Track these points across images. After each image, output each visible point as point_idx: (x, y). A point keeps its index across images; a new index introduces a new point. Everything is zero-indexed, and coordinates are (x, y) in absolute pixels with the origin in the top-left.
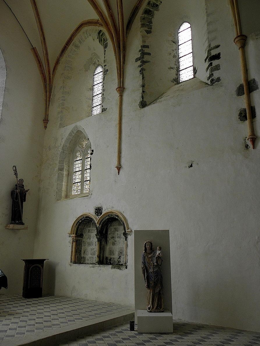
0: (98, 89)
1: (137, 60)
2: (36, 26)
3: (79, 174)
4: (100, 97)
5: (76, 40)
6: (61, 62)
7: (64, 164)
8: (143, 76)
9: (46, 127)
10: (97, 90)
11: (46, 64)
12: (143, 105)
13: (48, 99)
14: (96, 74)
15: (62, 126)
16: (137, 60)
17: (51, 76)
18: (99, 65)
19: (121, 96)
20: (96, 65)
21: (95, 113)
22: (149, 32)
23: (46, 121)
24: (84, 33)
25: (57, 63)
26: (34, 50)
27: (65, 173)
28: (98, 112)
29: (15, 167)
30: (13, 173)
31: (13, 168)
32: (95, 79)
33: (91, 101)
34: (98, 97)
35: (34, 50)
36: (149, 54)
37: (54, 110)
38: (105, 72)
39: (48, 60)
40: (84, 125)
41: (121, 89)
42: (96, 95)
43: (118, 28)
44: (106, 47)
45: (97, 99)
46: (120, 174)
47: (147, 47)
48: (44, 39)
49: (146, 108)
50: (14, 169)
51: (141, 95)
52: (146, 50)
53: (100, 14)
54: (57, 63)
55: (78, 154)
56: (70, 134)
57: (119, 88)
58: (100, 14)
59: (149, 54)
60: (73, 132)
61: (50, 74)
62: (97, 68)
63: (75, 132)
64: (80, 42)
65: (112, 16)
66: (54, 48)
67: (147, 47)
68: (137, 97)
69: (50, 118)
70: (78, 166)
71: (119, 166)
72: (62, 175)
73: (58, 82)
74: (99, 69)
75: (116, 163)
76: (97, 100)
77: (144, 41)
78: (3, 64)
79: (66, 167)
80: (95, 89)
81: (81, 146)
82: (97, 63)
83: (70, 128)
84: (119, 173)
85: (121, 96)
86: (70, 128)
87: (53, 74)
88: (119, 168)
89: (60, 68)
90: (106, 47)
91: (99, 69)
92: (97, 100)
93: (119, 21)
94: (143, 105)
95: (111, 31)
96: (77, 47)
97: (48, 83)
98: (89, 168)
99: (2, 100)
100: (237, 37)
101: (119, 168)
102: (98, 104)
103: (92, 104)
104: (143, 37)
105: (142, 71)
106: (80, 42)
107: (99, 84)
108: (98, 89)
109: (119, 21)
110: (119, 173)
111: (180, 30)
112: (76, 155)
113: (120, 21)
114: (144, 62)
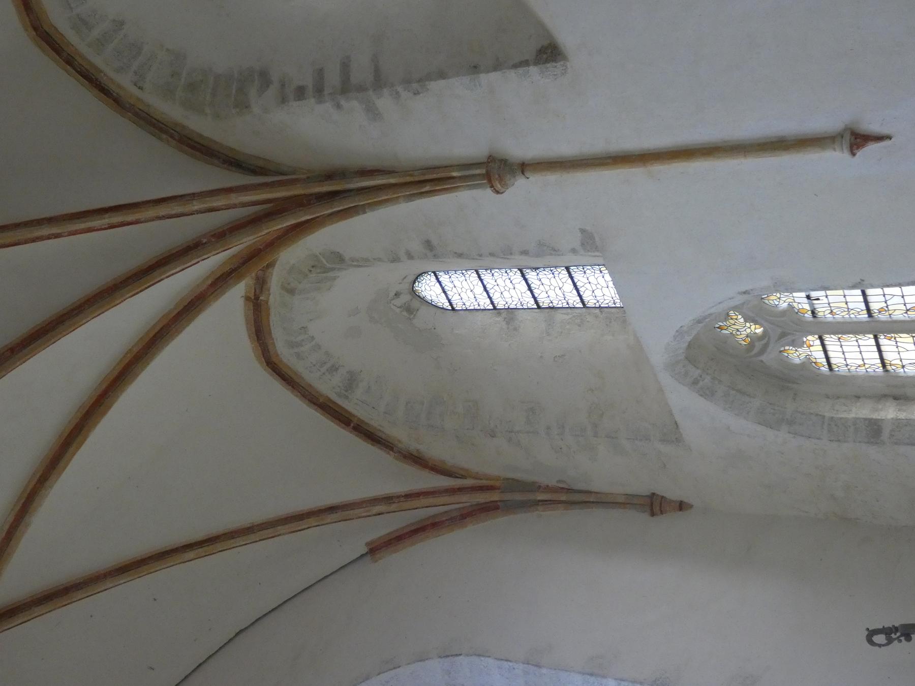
0: (508, 288)
1: (373, 113)
2: (286, 541)
3: (895, 349)
4: (540, 276)
5: (327, 387)
6: (413, 446)
7: (847, 419)
8: (429, 77)
9: (682, 506)
10: (512, 291)
11: (424, 501)
12: (549, 53)
13: (563, 497)
14: (449, 301)
15: (672, 434)
16: (373, 113)
17: (468, 482)
18: (413, 292)
19: (524, 167)
20: (416, 304)
21: (605, 291)
22: (265, 79)
23: (655, 505)
24: (298, 356)
25: (417, 460)
26: (375, 550)
27: (889, 413)
28: (600, 280)
29: (871, 634)
30: (900, 647)
31: (880, 646)
32: (468, 304)
33: (559, 316)
34: (539, 283)
35: (375, 550)
36: (345, 66)
37: (607, 471)
38: (439, 254)
39: (409, 496)
40: (660, 340)
41: (495, 171)
42: (534, 297)
43: (265, 206)
44: (338, 260)
45: (547, 288)
46: (885, 131)
47: (320, 74)
48: (332, 509)
49: (566, 39)
50: (880, 639)
51: (512, 74)
52: (333, 78)
53: (220, 282)
54: (417, 460)
55: (796, 355)
56: (708, 394)
57: (490, 181)
58: (220, 282)
59: (345, 66)
60: (695, 382)
61: (459, 484)
62: (423, 300)
63: (695, 373)
64: (334, 369)
65: (221, 236)
66: (369, 475)
67: (320, 74)
68: (515, 89)
69: (641, 486)
70: (854, 355)
71: (847, 137)
72: (898, 424)
73: (492, 459)
74: (427, 287)
75: (835, 159)
76: (553, 287)
77: (300, 93)
78: (435, 665)
79: (863, 411)
80: (510, 301)
81: (758, 346)
82: (405, 298)
83: (683, 400)
84: (880, 138)
85: (524, 167)
86: (683, 400)
87: (463, 477)
88: (857, 139)
89: (437, 449)
90: (338, 260)
91: (428, 288)
92: (553, 287)
93: (234, 206)
94: (549, 53)
95: (279, 238)
96: (352, 381)
97: (495, 496)
98: (859, 292)
99: (578, 679)
100: (492, 187)
101: (857, 139)
102: (570, 281)
103: (569, 311)
104: (283, 100)
105: (417, 81)
106: (334, 369)
107: (488, 286)
108: (508, 288)
109: (234, 206)
110: (880, 138)
111: (442, 301)
112: (784, 313)
113: (235, 199)
114: (379, 82)
